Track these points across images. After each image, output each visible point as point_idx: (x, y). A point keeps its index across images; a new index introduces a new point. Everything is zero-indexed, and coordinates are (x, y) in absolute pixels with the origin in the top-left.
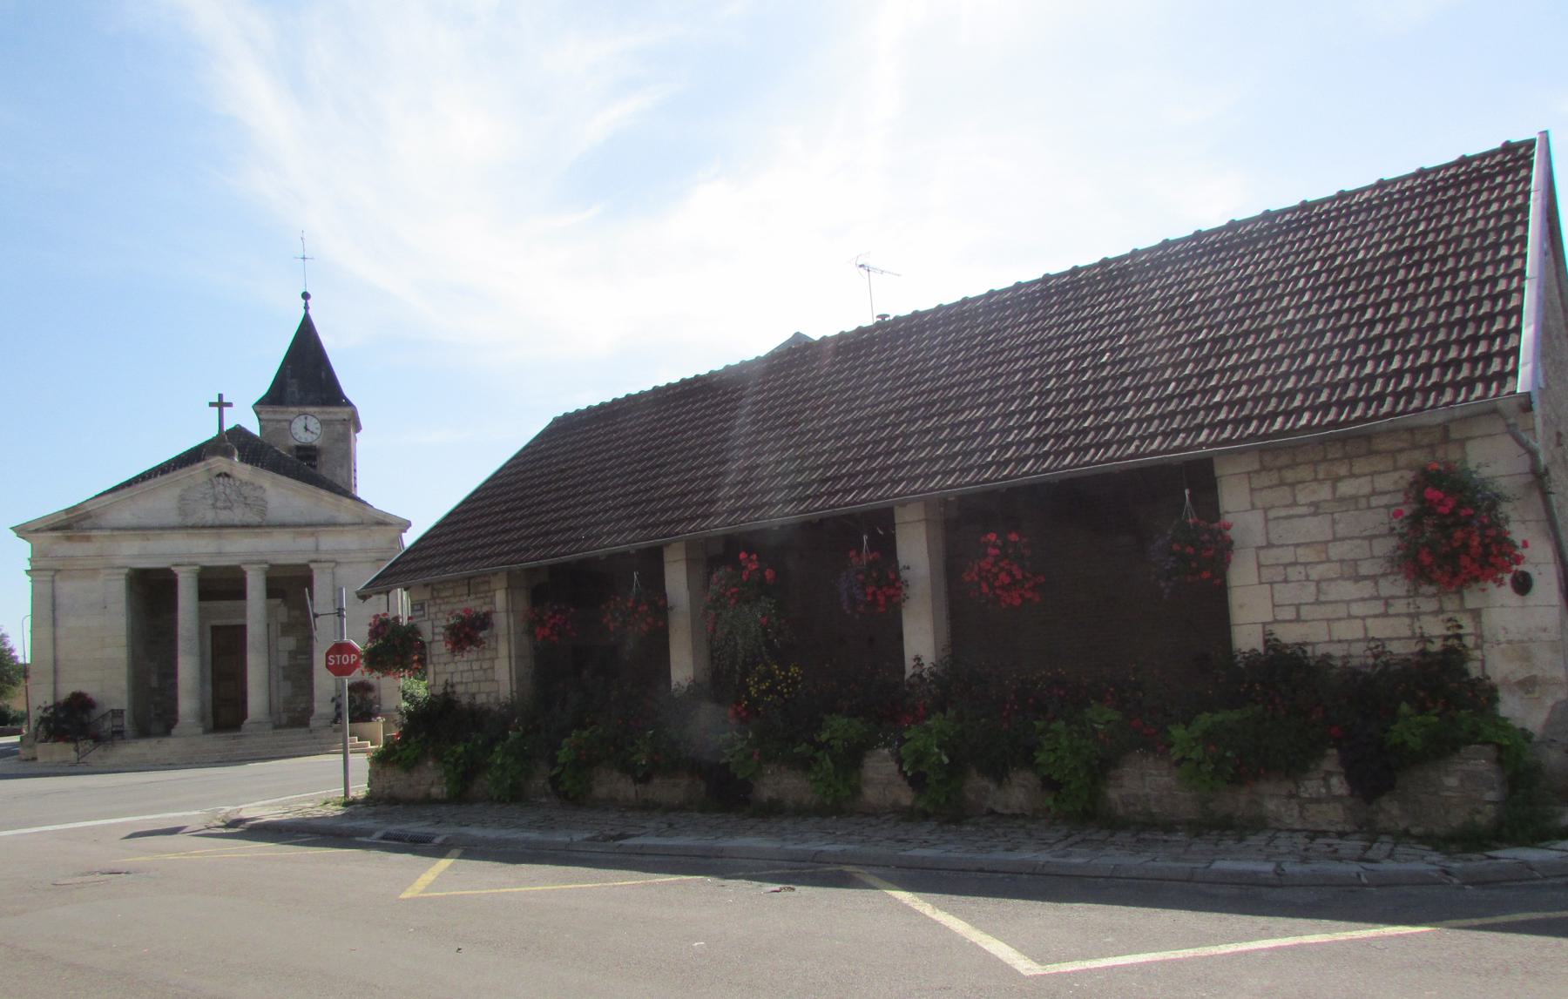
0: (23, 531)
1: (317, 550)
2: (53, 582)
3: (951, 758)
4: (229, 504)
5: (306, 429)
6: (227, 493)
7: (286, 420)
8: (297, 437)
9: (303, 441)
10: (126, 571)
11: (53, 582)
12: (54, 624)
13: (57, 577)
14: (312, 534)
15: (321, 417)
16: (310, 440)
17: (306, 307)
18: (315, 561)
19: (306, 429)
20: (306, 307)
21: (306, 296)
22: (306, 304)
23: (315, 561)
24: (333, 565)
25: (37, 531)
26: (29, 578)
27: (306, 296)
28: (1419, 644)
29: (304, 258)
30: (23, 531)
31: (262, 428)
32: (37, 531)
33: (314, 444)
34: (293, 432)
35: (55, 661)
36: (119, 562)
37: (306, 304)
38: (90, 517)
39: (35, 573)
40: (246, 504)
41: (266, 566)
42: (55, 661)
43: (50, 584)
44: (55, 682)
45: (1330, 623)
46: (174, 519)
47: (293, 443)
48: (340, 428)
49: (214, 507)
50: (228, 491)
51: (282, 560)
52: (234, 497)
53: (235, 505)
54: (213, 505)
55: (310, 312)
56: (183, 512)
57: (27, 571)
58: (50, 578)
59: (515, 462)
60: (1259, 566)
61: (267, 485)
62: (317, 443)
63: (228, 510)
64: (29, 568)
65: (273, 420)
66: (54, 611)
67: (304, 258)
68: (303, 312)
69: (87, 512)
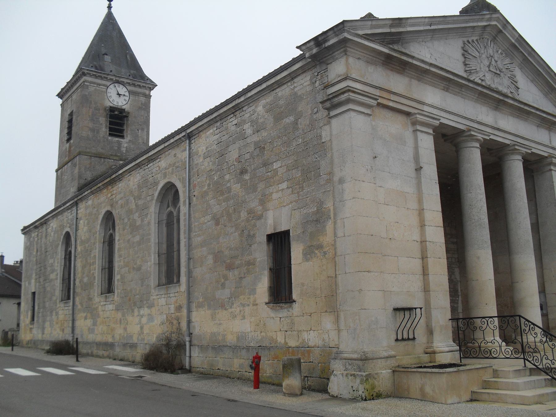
0: (57, 96)
3: (4, 269)
5: (119, 95)
7: (104, 85)
8: (111, 100)
9: (115, 103)
16: (120, 104)
17: (110, 7)
19: (119, 95)
20: (110, 7)
28: (171, 344)
30: (57, 96)
31: (301, 50)
33: (124, 107)
34: (109, 95)
45: (261, 379)
47: (108, 104)
55: (113, 10)
59: (60, 159)
62: (127, 107)
65: (94, 83)
68: (106, 11)
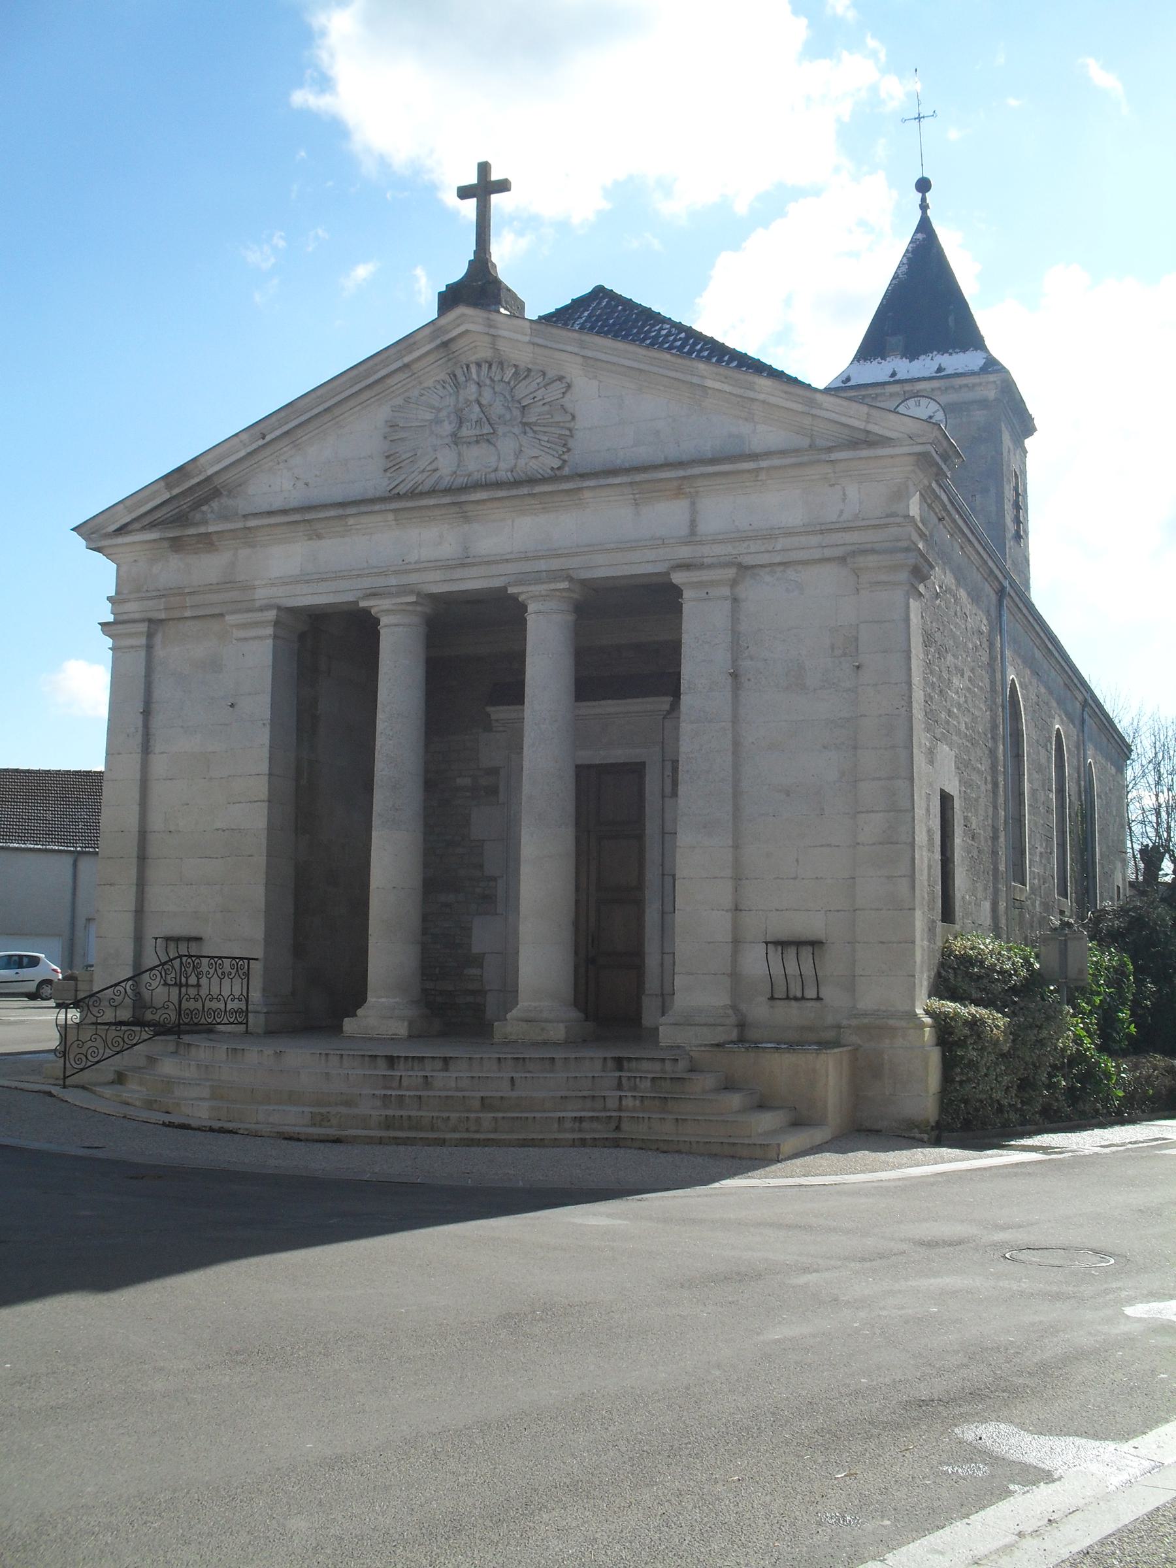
1: (692, 536)
2: (149, 647)
4: (487, 429)
6: (484, 402)
10: (272, 615)
11: (149, 647)
12: (146, 748)
13: (158, 639)
14: (679, 493)
15: (944, 399)
17: (924, 206)
18: (686, 566)
20: (924, 206)
21: (923, 185)
22: (924, 199)
23: (686, 566)
24: (731, 572)
25: (122, 530)
26: (109, 642)
27: (923, 185)
29: (919, 118)
32: (122, 530)
35: (143, 835)
36: (262, 595)
37: (924, 199)
38: (216, 493)
39: (121, 629)
40: (525, 424)
41: (565, 585)
42: (143, 835)
43: (143, 654)
44: (141, 884)
46: (372, 480)
48: (980, 416)
49: (456, 439)
50: (487, 396)
51: (605, 567)
52: (498, 409)
53: (501, 430)
54: (454, 435)
56: (392, 462)
57: (103, 625)
58: (143, 641)
60: (247, 1024)
61: (574, 370)
63: (484, 445)
64: (110, 618)
66: (147, 713)
67: (919, 118)
69: (208, 479)
